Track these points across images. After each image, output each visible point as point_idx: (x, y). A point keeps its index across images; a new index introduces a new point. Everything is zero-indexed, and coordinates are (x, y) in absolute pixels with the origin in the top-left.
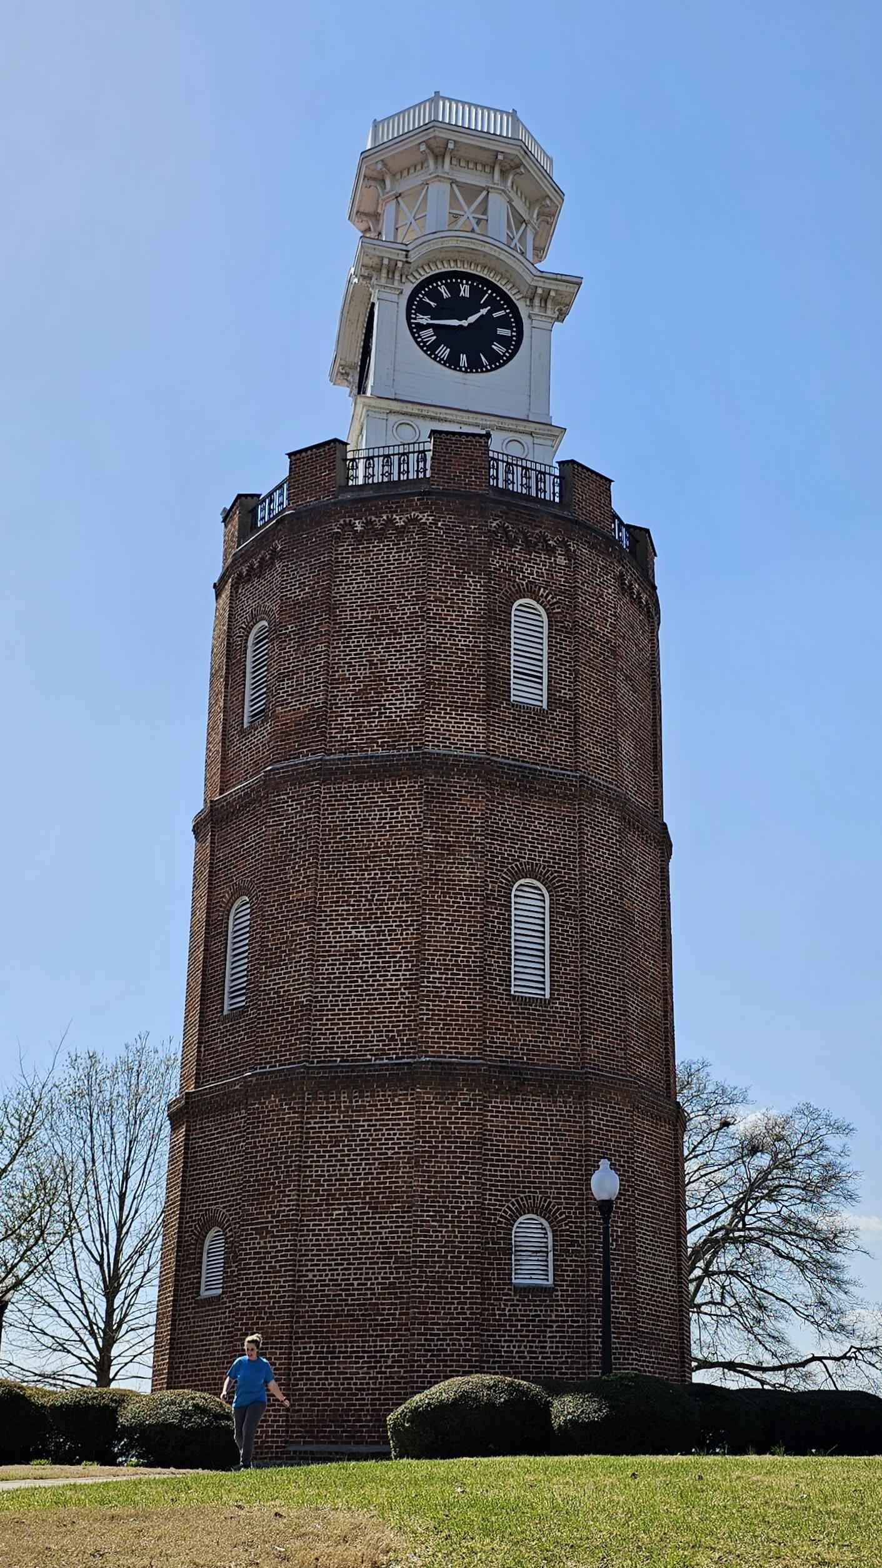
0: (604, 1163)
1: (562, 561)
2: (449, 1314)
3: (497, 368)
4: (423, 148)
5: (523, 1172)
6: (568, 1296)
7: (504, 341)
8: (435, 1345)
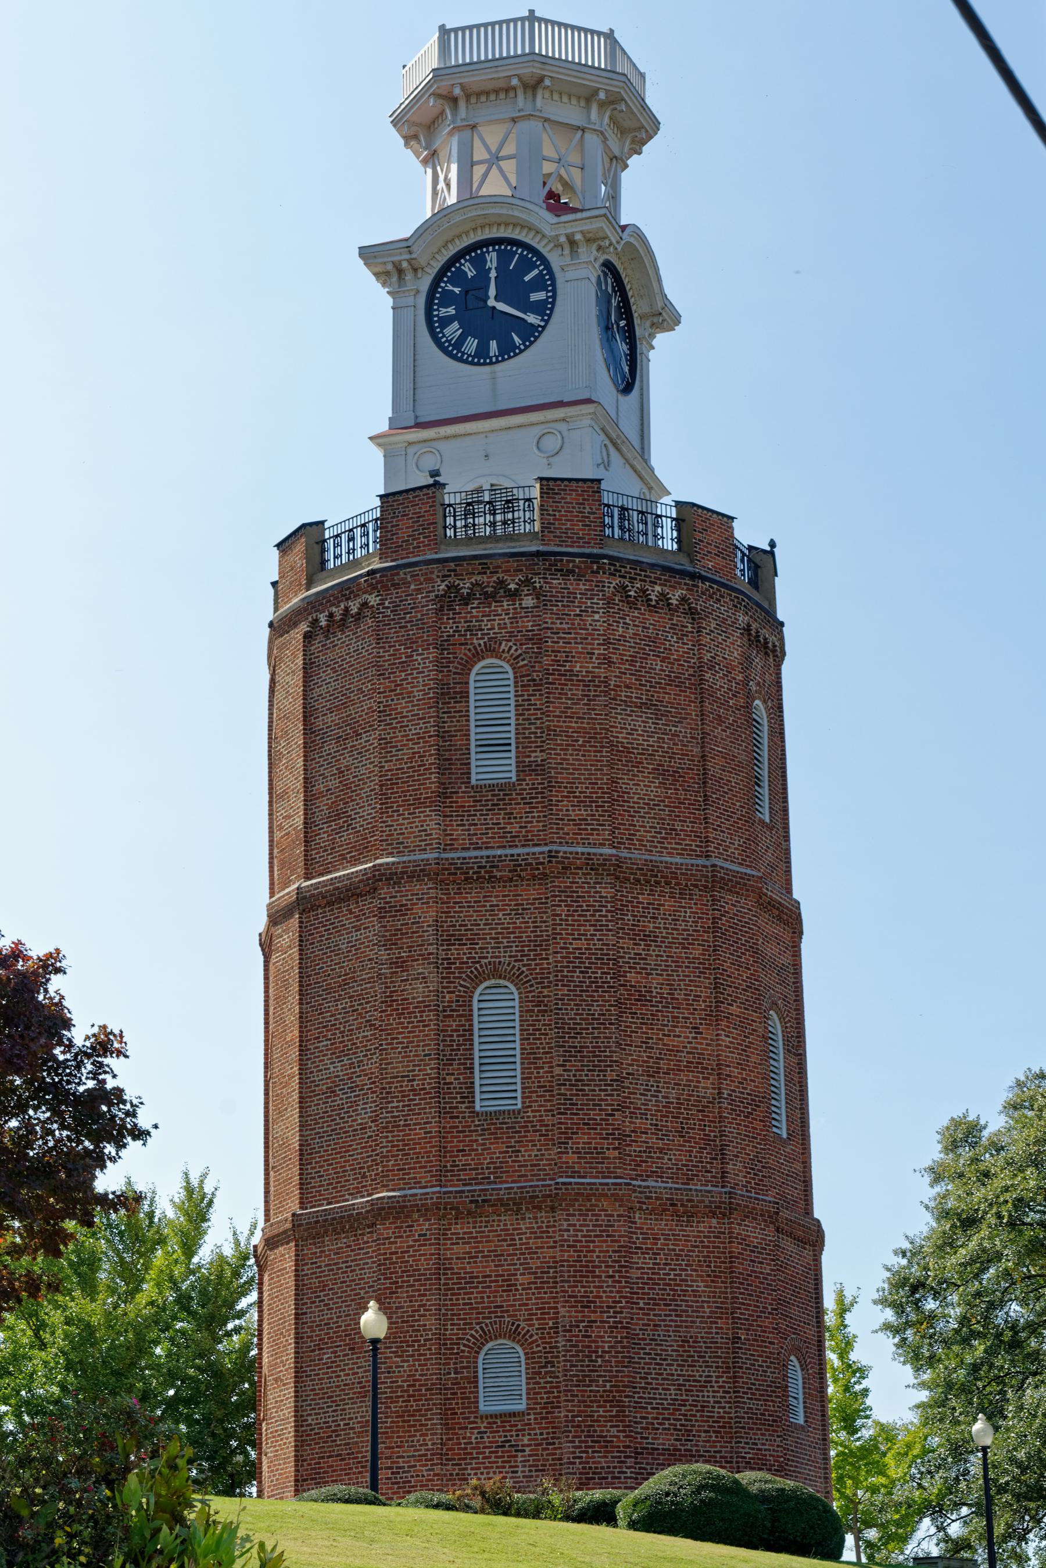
1: (529, 602)
2: (412, 1446)
5: (489, 1297)
6: (542, 1418)
8: (401, 1478)
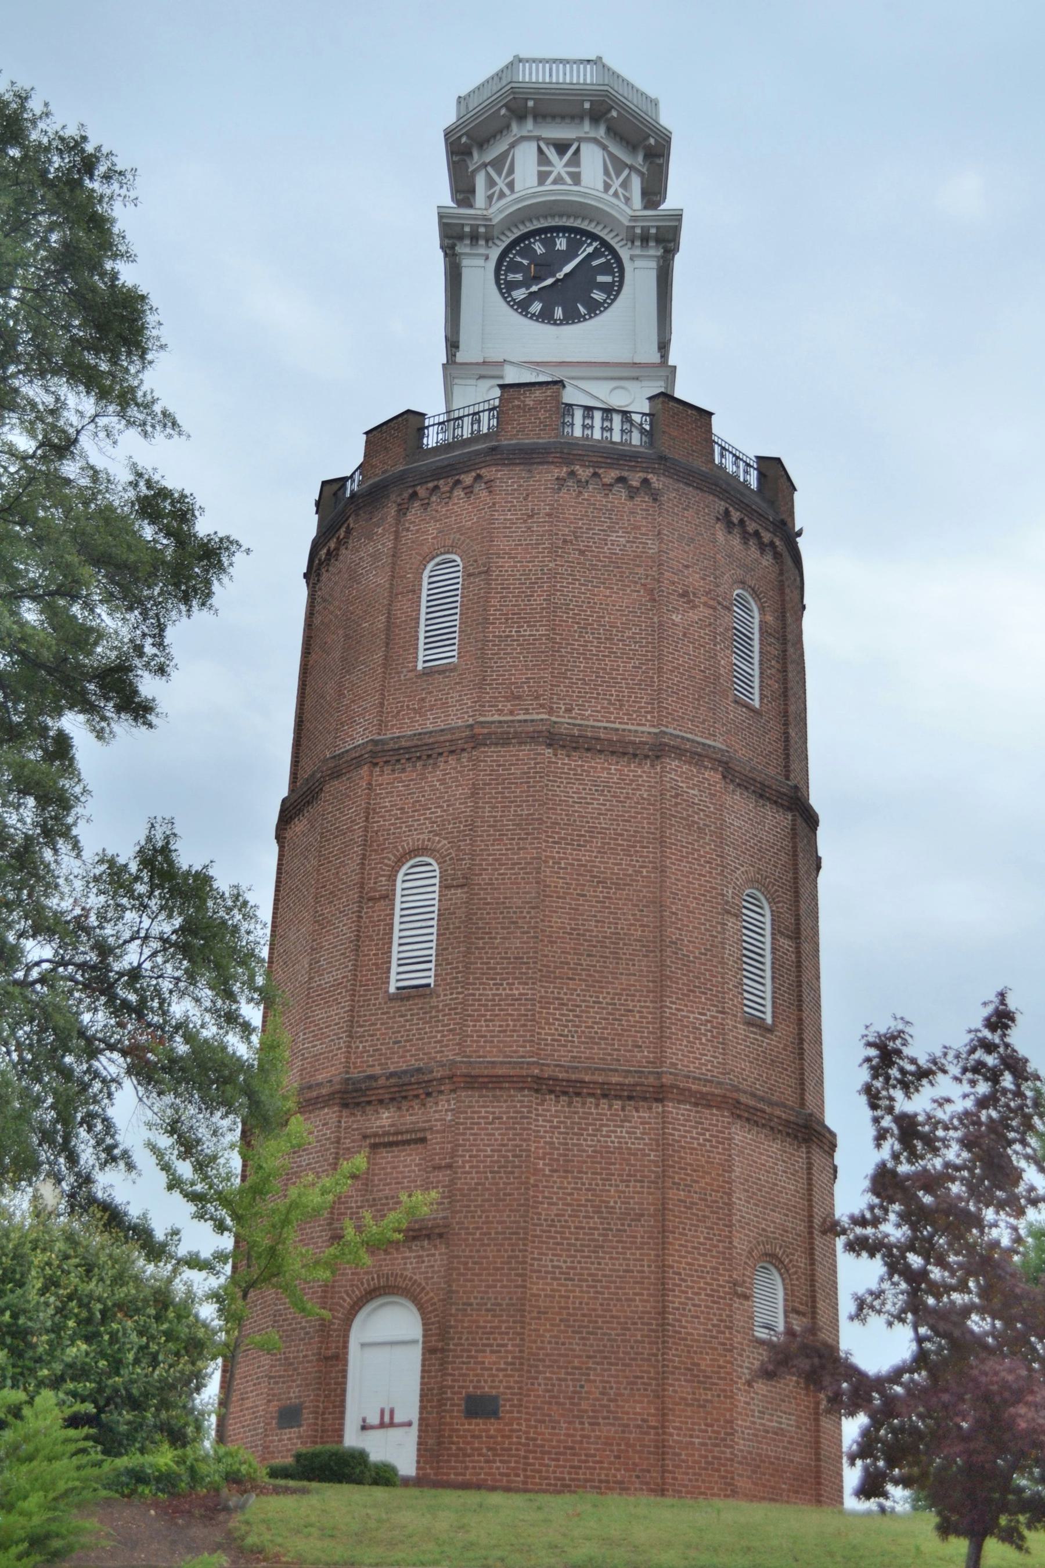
0: (908, 1254)
3: (616, 296)
4: (503, 111)
7: (605, 288)
